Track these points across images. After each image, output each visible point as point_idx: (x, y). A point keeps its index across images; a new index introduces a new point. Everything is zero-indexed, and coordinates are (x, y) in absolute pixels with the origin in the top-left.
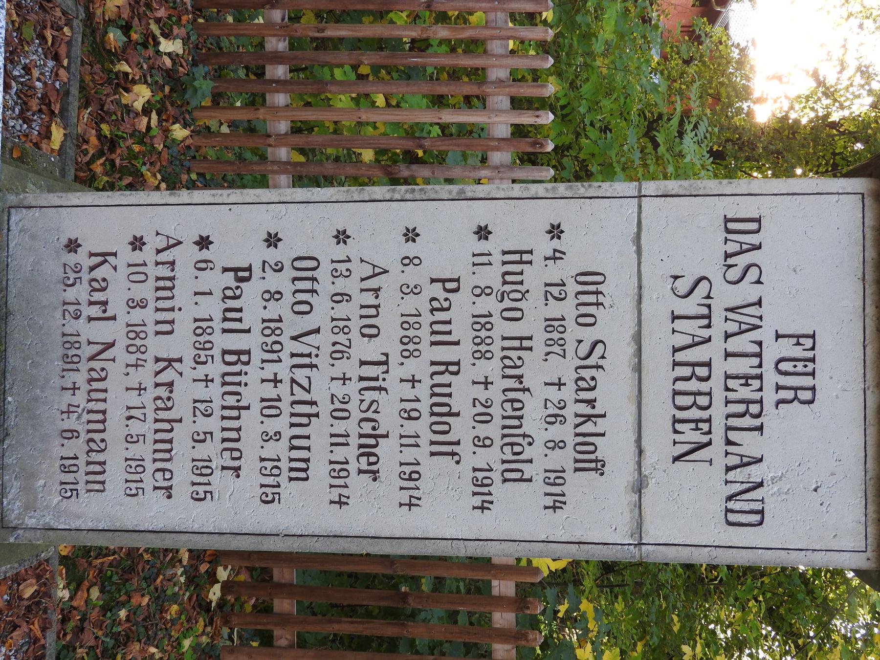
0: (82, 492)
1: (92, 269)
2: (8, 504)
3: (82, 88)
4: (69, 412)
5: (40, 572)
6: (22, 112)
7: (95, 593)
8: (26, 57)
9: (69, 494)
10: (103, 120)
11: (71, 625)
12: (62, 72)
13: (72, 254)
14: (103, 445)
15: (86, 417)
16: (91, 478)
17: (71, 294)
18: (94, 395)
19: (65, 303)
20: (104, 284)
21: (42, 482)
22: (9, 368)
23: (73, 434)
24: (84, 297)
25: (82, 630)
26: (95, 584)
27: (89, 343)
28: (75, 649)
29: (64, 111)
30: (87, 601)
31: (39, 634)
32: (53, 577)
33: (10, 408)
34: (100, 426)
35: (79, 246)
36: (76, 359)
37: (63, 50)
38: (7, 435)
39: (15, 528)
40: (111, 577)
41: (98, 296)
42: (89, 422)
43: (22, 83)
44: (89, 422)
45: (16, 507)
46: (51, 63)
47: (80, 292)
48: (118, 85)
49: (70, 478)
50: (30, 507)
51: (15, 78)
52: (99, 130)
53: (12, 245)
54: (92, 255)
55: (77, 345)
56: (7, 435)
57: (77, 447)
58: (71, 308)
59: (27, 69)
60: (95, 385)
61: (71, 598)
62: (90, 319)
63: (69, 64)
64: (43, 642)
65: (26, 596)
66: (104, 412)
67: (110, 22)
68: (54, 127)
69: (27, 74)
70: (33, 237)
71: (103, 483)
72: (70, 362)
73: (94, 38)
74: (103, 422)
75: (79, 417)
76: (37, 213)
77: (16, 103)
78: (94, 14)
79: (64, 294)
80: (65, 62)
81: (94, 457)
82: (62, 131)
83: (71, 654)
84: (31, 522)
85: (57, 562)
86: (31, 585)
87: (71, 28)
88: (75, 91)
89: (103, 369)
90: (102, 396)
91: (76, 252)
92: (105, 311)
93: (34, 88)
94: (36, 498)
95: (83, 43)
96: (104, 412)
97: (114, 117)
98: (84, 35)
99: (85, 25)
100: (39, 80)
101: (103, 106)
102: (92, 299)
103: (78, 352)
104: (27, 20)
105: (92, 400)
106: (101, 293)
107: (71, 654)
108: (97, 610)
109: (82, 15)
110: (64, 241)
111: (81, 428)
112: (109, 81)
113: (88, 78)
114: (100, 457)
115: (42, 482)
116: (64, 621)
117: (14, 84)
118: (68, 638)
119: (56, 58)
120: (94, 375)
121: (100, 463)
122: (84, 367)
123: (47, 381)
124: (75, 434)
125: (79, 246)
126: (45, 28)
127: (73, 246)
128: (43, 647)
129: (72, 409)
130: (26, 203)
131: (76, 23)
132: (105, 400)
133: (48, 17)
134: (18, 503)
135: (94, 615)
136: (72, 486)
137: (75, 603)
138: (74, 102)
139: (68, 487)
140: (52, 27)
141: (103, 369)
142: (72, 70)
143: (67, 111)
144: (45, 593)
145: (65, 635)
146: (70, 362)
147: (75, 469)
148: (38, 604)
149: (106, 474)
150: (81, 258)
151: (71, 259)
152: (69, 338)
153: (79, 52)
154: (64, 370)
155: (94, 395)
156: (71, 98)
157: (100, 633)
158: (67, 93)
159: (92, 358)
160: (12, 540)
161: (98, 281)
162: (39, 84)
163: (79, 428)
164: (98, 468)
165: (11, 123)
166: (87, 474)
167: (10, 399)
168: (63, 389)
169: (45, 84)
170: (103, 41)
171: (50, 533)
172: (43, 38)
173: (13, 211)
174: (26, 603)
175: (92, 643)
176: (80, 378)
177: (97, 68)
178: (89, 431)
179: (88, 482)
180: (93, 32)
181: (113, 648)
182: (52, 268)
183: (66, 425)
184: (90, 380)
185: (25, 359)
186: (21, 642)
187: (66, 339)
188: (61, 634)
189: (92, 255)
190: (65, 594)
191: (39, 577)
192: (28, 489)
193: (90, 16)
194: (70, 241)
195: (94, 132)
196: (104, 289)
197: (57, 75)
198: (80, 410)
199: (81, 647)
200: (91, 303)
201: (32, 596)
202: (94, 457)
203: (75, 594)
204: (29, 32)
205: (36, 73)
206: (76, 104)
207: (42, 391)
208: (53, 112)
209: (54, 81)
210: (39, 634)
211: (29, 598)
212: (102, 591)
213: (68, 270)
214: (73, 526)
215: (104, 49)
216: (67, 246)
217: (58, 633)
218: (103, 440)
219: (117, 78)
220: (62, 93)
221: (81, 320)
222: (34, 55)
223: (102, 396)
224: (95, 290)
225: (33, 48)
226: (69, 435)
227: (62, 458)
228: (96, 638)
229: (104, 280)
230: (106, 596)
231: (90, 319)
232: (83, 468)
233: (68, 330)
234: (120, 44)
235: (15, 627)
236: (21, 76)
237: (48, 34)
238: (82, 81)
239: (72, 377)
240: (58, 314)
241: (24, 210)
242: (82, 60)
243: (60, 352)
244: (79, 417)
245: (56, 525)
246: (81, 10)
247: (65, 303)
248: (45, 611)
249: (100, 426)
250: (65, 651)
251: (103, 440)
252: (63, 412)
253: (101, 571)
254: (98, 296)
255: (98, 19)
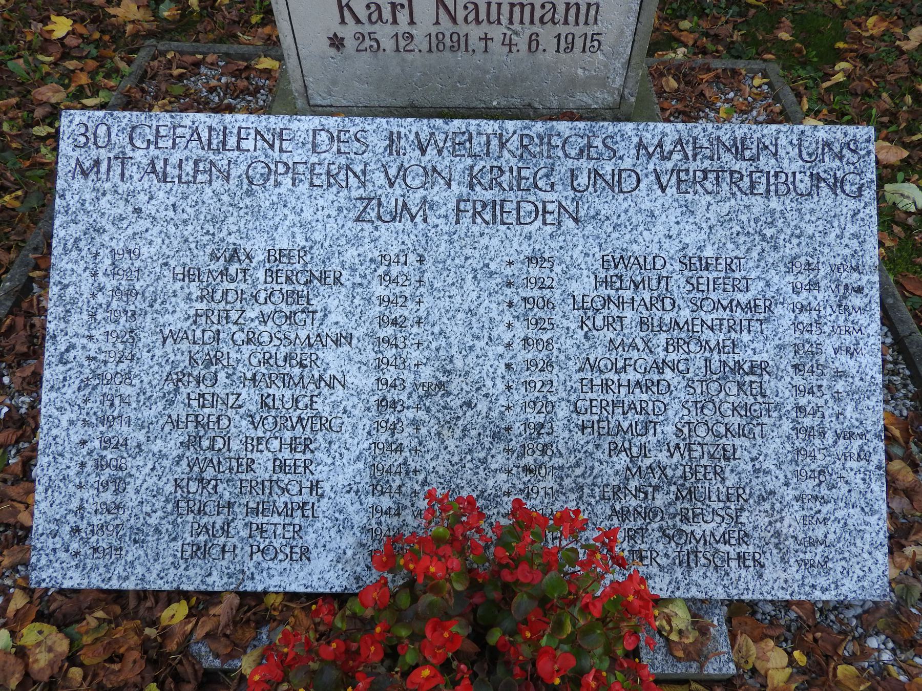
0: (596, 29)
1: (358, 21)
2: (597, 103)
3: (221, 41)
4: (510, 45)
5: (657, 74)
6: (250, 94)
7: (685, 24)
8: (201, 92)
9: (596, 43)
10: (248, 22)
11: (710, 47)
12: (210, 58)
13: (345, 42)
14: (548, 6)
15: (517, 26)
16: (582, 19)
17: (387, 44)
18: (493, 17)
19: (398, 50)
20: (373, 8)
21: (580, 72)
22: (465, 104)
23: (533, 39)
24: (389, 29)
25: (716, 35)
26: (677, 24)
27: (437, 23)
28: (733, 42)
29: (243, 58)
30: (691, 31)
31: (712, 74)
32: (664, 63)
33: (504, 103)
34: (527, 10)
35: (335, 35)
36: (455, 38)
37: (189, 59)
38: (530, 105)
39: (622, 97)
40: (673, 10)
41: (387, 14)
42: (522, 22)
43: (225, 95)
44: (522, 22)
45: (601, 96)
46: (203, 70)
47: (384, 32)
48: (213, 7)
49: (579, 43)
50: (603, 83)
51: (221, 100)
52: (258, 25)
53: (345, 103)
54: (343, 22)
55: (441, 36)
56: (530, 105)
57: (547, 34)
58: (402, 43)
59: (212, 90)
60: (483, 16)
61: (686, 46)
62: (412, 22)
63: (200, 53)
64: (720, 71)
65: (676, 85)
66: (512, 5)
67: (155, 14)
68: (259, 67)
69: (215, 90)
70: (334, 82)
71: (589, 5)
72: (459, 44)
73: (172, 30)
74: (522, 6)
75: (517, 34)
76: (309, 79)
77: (243, 99)
78: (149, 30)
79: (388, 51)
80: (200, 57)
81: (559, 16)
82: (263, 59)
83: (736, 45)
84: (619, 81)
85: (651, 59)
86: (667, 81)
87: (167, 51)
88: (224, 48)
89: (466, 7)
90: (494, 8)
91: (343, 39)
92: (402, 6)
93: (227, 84)
94: (594, 77)
95: (178, 41)
96: (512, 5)
97: (243, 11)
98: (171, 40)
99: (162, 38)
100: (219, 80)
101: (234, 22)
102: (391, 20)
103: (448, 35)
104: (167, 91)
105: (499, 19)
106: (383, 10)
107: (736, 45)
108: (701, 22)
109: (153, 41)
110: (333, 52)
111: (528, 30)
112: (211, 16)
113: (211, 36)
114: (561, 9)
115: (580, 72)
116: (704, 52)
117: (226, 101)
118: (721, 48)
119: (197, 64)
120: (471, 17)
121: (567, 10)
122: (463, 29)
123: (478, 67)
124: (534, 37)
125: (335, 35)
126: (171, 75)
127: (336, 42)
128: (724, 70)
129: (507, 41)
130: (302, 90)
131: (160, 47)
132: (499, 5)
133: (161, 72)
134: (598, 95)
135: (705, 24)
136: (589, 40)
137: (691, 43)
138: (234, 48)
139: (588, 44)
140: (170, 69)
141: (466, 7)
142: (205, 50)
143: (243, 55)
144: (676, 70)
145: (717, 51)
146: (459, 44)
147: (570, 37)
148: (685, 75)
149: (580, 2)
150: (348, 32)
151: (350, 44)
152: (434, 45)
153: (188, 44)
154: (467, 50)
155: (493, 17)
156: (232, 51)
157: (723, 19)
158: (227, 55)
159: (454, 20)
160: (633, 99)
161: (370, 15)
162: (224, 80)
163: (528, 33)
164: (573, 12)
165: (261, 103)
166: (577, 23)
167: (495, 103)
168: (486, 51)
169: (222, 74)
170: (173, 22)
171: (633, 62)
172: (181, 77)
173: (312, 102)
174: (682, 86)
175: (730, 27)
176: (475, 32)
177: (200, 27)
178: (532, 22)
179: (586, 23)
180: (168, 31)
181: (740, 7)
182: (363, 63)
183: (524, 47)
184: (478, 21)
185: (456, 90)
186: (715, 89)
187: (434, 49)
188: (717, 55)
189: (343, 22)
190: (681, 51)
191: (662, 75)
192: (585, 85)
193: (151, 34)
194: (332, 45)
195: (260, 30)
196: (378, 7)
197: (212, 64)
198: (509, 33)
199: (732, 37)
200: (395, 22)
201: (678, 80)
202: (559, 16)
203: (682, 42)
204: (178, 89)
205: (213, 83)
206: (236, 46)
207: (488, 72)
208: (247, 68)
209: (219, 66)
210: (712, 74)
211: (679, 83)
212: (684, 18)
213: (362, 47)
214: (630, 38)
215: (180, 21)
216: (338, 49)
217: (715, 57)
218: (543, 6)
219: (205, 8)
220: (228, 60)
221: (414, 32)
222: (198, 85)
223: (494, 8)
224: (380, 17)
225: (192, 85)
226: (534, 43)
227: (558, 51)
228: (727, 22)
229: (368, 7)
230: (690, 14)
231: (412, 22)
232: (571, 28)
233: (425, 46)
234: (173, 5)
235: (702, 94)
236: (219, 95)
237: (176, 72)
238: (214, 41)
239: (474, 42)
240: (409, 57)
241: (310, 92)
242: (195, 41)
243: (447, 54)
244: (517, 34)
245: (626, 57)
246: (148, 42)
247: (398, 50)
248: (692, 69)
249: (527, 10)
250: (733, 51)
251: (543, 6)
252: (510, 51)
253: (666, 19)
254: (387, 14)
255: (153, 26)
